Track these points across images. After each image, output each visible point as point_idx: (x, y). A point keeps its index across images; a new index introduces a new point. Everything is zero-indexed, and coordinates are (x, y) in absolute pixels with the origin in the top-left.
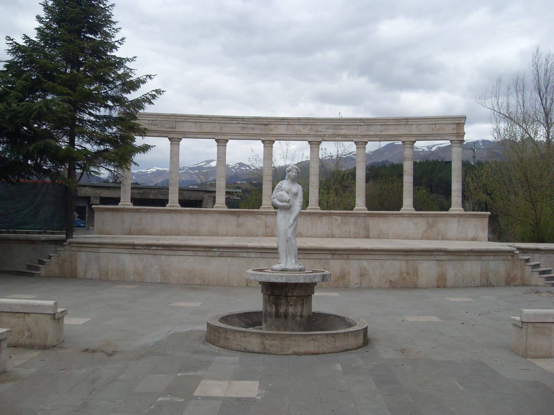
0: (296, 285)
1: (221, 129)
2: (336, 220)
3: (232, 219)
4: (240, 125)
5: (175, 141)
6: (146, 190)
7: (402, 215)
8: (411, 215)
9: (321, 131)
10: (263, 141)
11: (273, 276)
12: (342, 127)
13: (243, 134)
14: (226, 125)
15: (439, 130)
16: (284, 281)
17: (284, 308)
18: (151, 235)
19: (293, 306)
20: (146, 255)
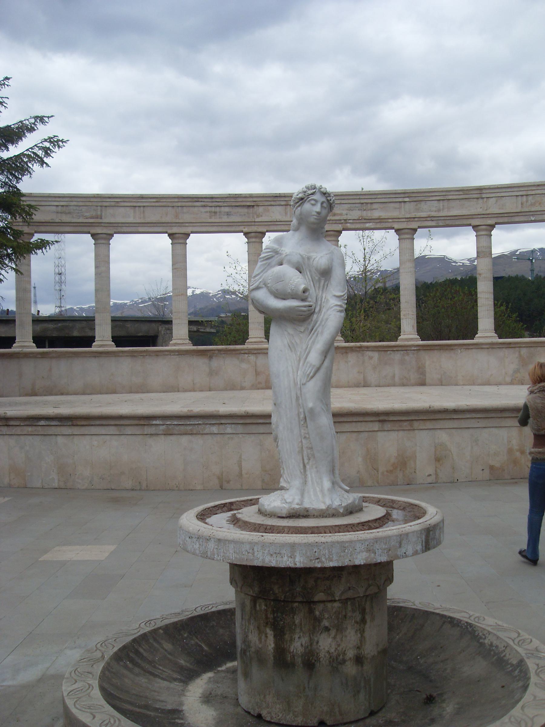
0: (337, 572)
1: (177, 216)
2: (371, 358)
3: (201, 363)
4: (208, 209)
5: (102, 239)
6: (67, 324)
7: (478, 346)
8: (492, 346)
9: (341, 214)
10: (246, 234)
11: (264, 545)
12: (375, 206)
13: (212, 224)
14: (185, 210)
15: (533, 205)
16: (299, 561)
17: (305, 640)
18: (67, 394)
19: (333, 632)
20: (30, 438)
